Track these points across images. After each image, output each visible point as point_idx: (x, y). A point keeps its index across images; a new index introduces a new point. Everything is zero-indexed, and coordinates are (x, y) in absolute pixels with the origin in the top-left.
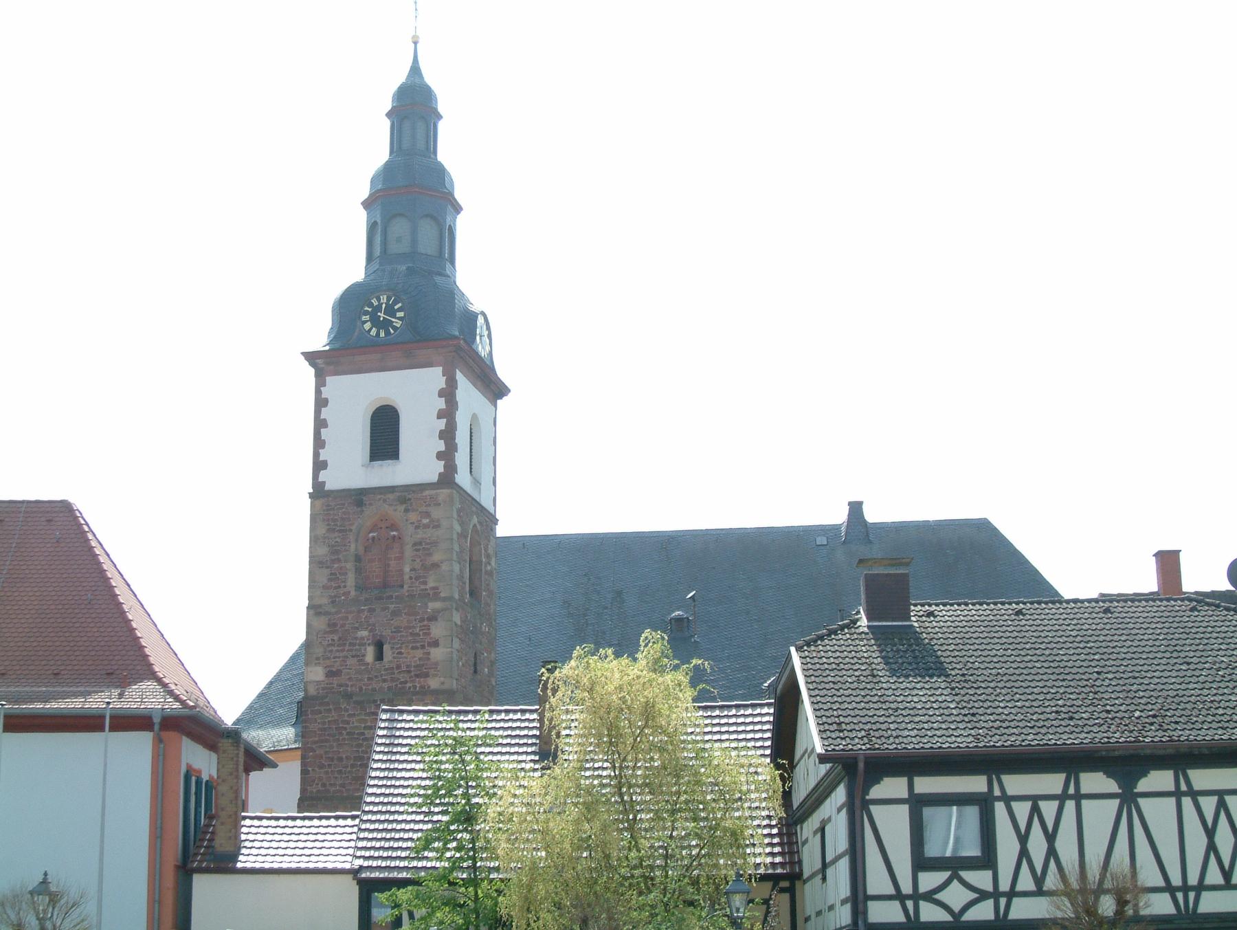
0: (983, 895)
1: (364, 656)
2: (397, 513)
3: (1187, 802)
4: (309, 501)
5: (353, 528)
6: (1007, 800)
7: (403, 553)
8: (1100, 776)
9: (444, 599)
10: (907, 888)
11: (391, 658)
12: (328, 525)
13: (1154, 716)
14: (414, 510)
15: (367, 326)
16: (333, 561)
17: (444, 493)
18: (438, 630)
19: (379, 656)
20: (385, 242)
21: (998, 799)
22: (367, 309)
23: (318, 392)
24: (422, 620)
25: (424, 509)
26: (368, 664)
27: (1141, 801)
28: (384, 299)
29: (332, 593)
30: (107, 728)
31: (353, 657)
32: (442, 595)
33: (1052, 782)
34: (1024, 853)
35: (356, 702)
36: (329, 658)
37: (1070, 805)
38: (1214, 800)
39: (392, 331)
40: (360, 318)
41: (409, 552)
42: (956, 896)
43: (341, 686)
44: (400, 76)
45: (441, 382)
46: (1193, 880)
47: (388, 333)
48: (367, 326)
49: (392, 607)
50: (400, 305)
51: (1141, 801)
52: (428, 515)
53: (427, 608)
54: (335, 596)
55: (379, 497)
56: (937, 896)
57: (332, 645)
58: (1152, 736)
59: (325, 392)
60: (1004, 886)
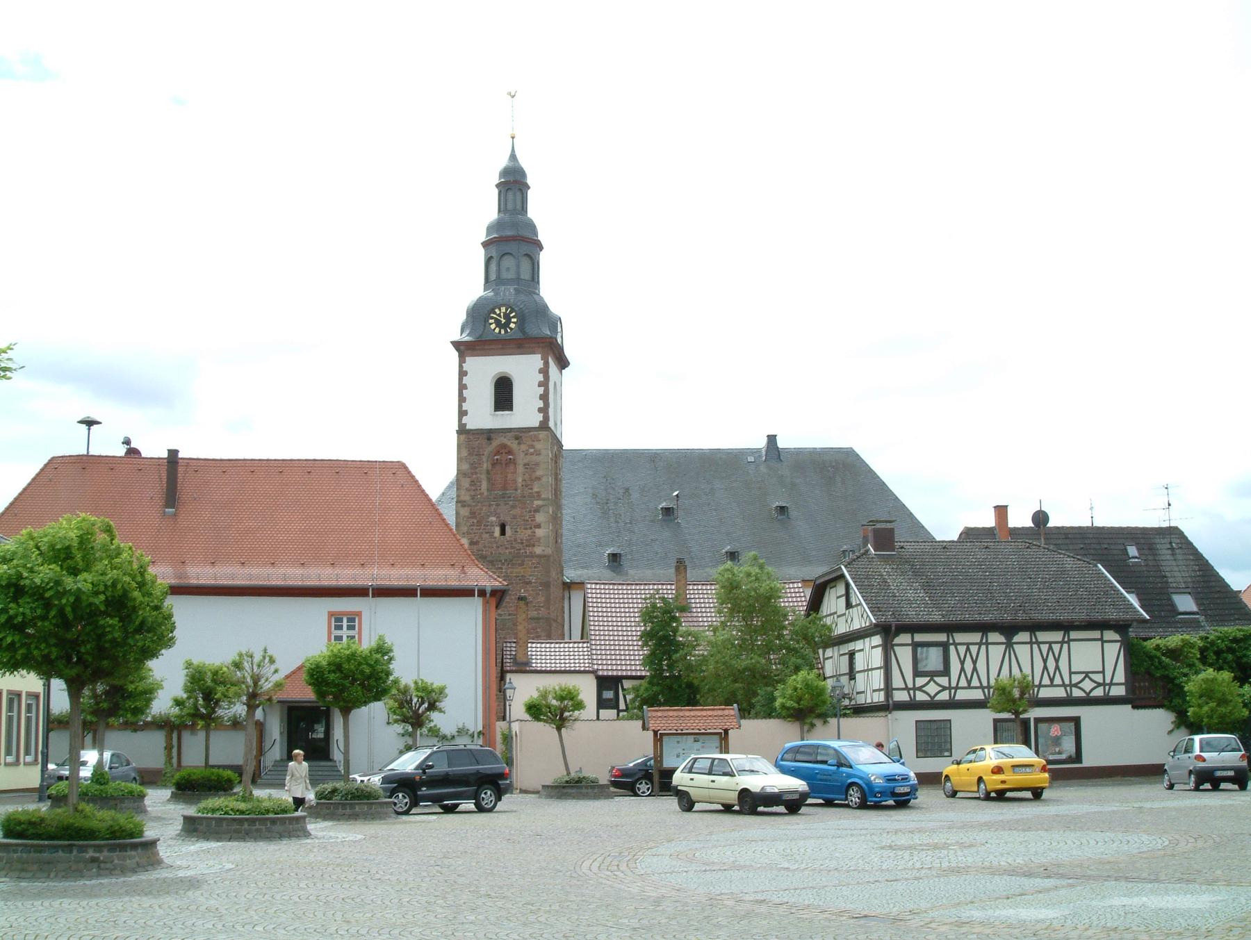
0: (1099, 685)
1: (493, 532)
2: (513, 445)
3: (1035, 646)
4: (456, 435)
9: (544, 500)
10: (910, 685)
13: (1020, 606)
14: (524, 444)
15: (493, 326)
17: (542, 434)
18: (540, 518)
19: (503, 532)
20: (499, 271)
21: (952, 644)
23: (461, 367)
24: (530, 512)
25: (530, 443)
26: (496, 538)
27: (1014, 646)
28: (503, 309)
29: (473, 493)
30: (476, 595)
31: (486, 533)
32: (543, 496)
33: (976, 637)
35: (488, 561)
36: (471, 534)
37: (983, 647)
39: (509, 331)
40: (488, 321)
41: (520, 469)
42: (932, 689)
43: (479, 551)
44: (503, 162)
45: (540, 364)
47: (506, 332)
48: (493, 326)
50: (514, 314)
51: (1014, 646)
52: (532, 447)
57: (474, 525)
58: (1021, 617)
60: (954, 684)
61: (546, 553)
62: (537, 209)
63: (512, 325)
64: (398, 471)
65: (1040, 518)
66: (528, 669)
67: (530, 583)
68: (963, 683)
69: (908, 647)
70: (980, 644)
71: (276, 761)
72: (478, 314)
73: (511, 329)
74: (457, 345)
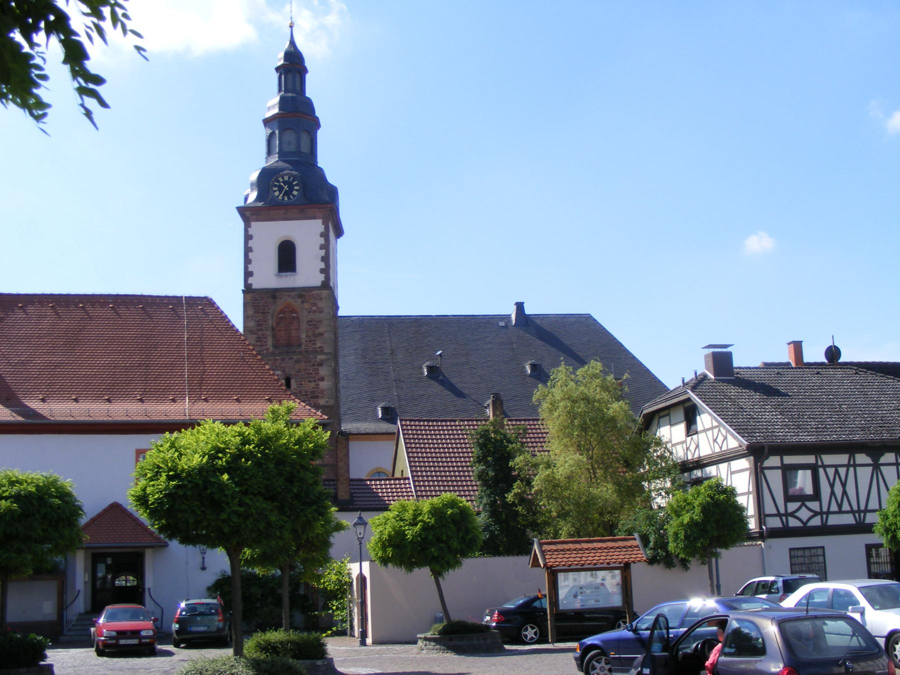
0: (816, 514)
2: (297, 303)
5: (270, 311)
6: (825, 467)
7: (299, 326)
8: (864, 455)
9: (327, 354)
10: (782, 511)
11: (295, 388)
12: (255, 309)
14: (307, 302)
15: (277, 193)
16: (258, 330)
17: (325, 293)
18: (324, 371)
21: (820, 466)
22: (276, 183)
23: (246, 231)
24: (314, 365)
32: (325, 351)
33: (843, 459)
34: (833, 493)
37: (852, 469)
38: (833, 469)
39: (292, 197)
40: (272, 189)
41: (304, 326)
42: (804, 514)
45: (321, 228)
46: (862, 507)
47: (289, 198)
49: (295, 357)
50: (296, 182)
52: (315, 305)
53: (317, 358)
54: (260, 351)
55: (286, 293)
56: (812, 514)
59: (251, 231)
60: (825, 509)
61: (328, 404)
62: (313, 89)
63: (295, 193)
64: (208, 303)
65: (833, 353)
66: (351, 507)
68: (834, 508)
69: (859, 463)
70: (848, 466)
71: (80, 614)
72: (266, 180)
73: (294, 196)
74: (242, 211)
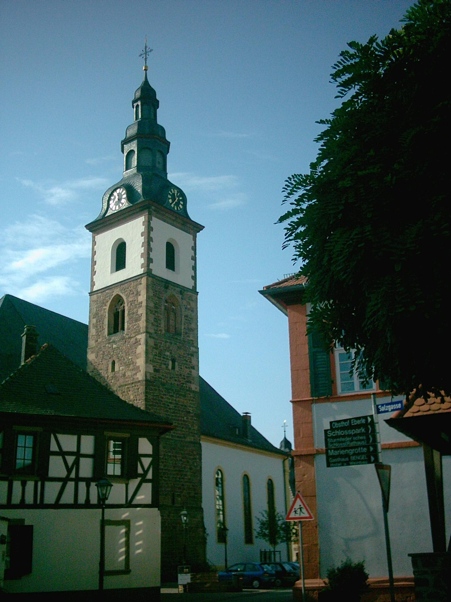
21: (55, 453)
44: (282, 439)
67: (189, 412)
